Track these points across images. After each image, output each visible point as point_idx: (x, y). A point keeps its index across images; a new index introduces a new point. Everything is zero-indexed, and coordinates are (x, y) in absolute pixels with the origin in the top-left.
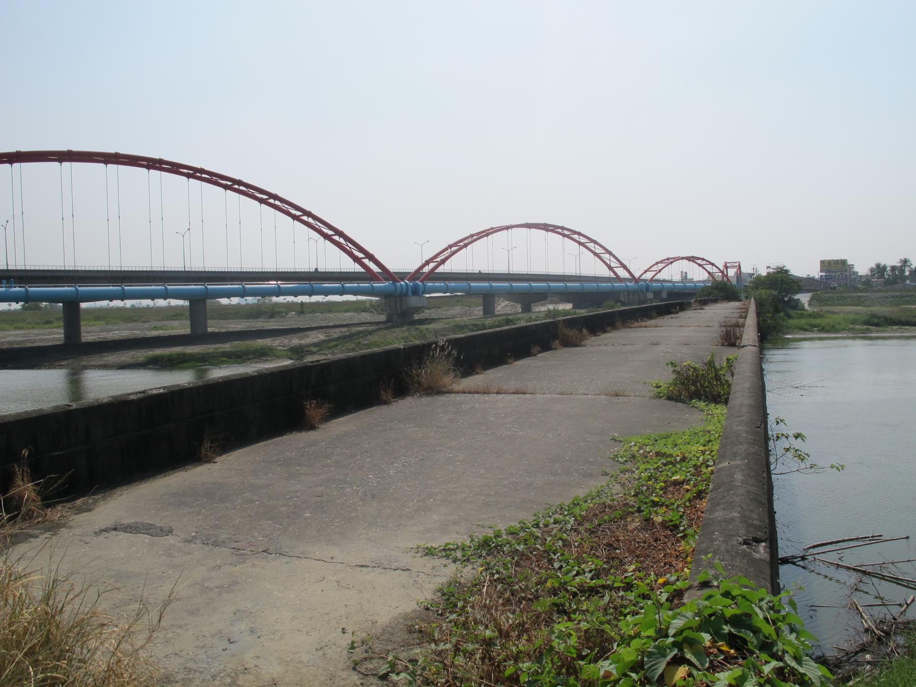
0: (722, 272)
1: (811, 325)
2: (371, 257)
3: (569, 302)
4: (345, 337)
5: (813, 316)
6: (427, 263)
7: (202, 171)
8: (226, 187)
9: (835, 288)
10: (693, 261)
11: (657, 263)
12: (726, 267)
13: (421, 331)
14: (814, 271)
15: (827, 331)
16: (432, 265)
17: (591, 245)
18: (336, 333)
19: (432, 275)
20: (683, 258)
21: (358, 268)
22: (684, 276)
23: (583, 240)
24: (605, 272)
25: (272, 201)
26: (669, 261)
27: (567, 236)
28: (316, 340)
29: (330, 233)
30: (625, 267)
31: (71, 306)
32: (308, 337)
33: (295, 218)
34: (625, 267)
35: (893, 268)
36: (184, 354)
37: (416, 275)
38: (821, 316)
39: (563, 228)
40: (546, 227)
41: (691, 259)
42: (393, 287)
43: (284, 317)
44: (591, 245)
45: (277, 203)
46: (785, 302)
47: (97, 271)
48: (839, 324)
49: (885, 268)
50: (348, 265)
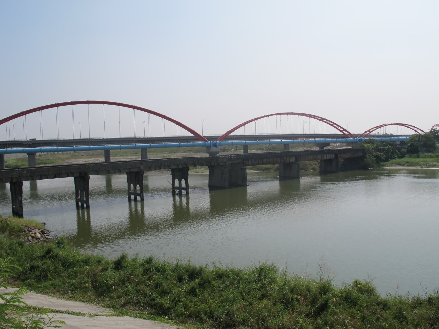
2: (346, 130)
6: (366, 132)
7: (314, 116)
8: (320, 120)
16: (367, 133)
19: (227, 137)
21: (341, 133)
27: (409, 128)
30: (422, 131)
31: (31, 154)
34: (422, 131)
47: (169, 137)
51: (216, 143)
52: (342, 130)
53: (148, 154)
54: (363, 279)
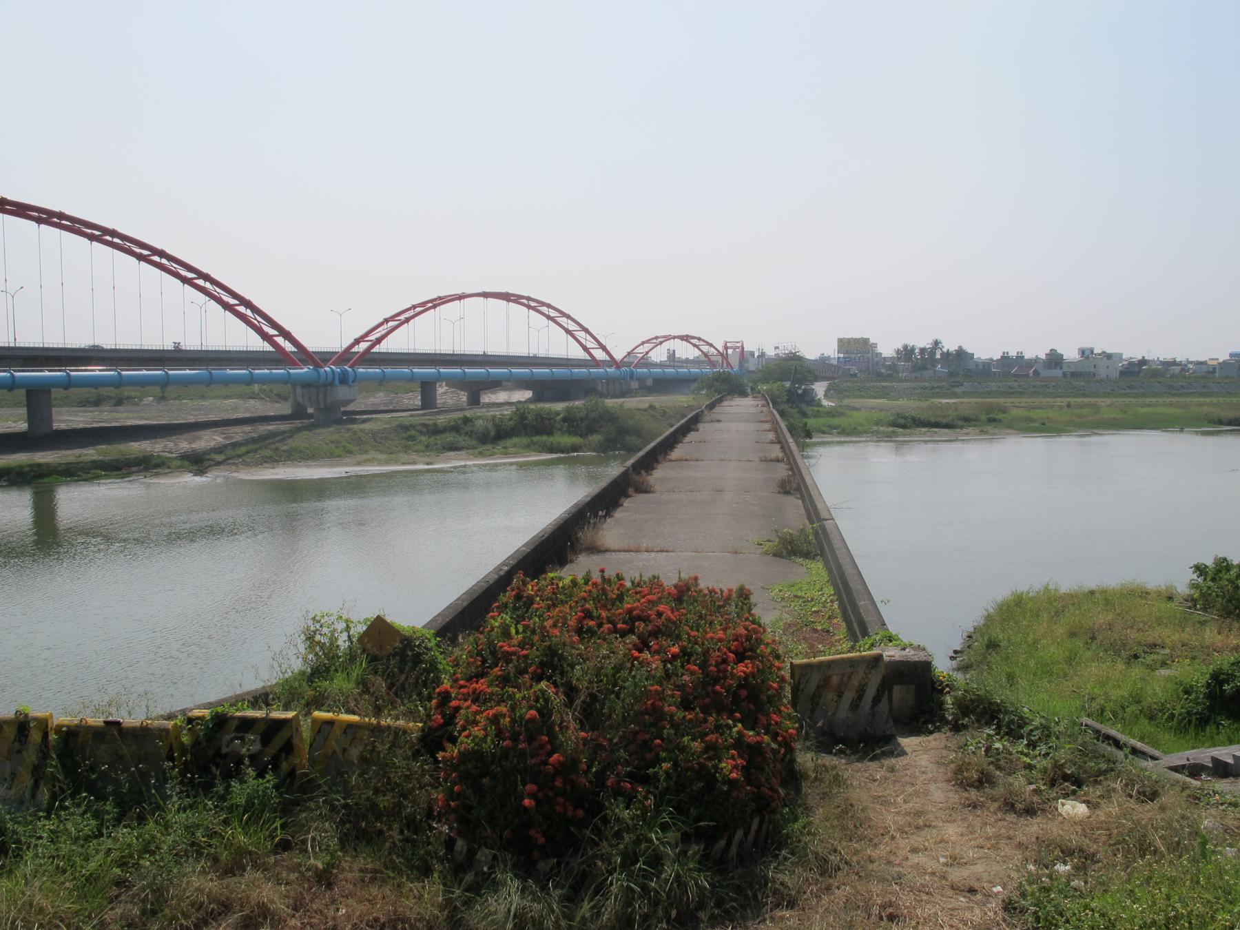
0: (722, 355)
1: (830, 426)
2: (287, 335)
3: (527, 388)
4: (254, 441)
5: (832, 413)
6: (357, 342)
7: (61, 216)
8: (92, 238)
9: (855, 375)
10: (687, 341)
11: (643, 343)
12: (726, 348)
13: (355, 433)
14: (831, 351)
15: (848, 434)
17: (563, 320)
18: (239, 434)
19: (367, 357)
20: (674, 337)
21: (268, 347)
22: (672, 355)
23: (553, 313)
24: (577, 353)
25: (156, 258)
26: (658, 341)
27: (534, 308)
28: (212, 444)
29: (233, 301)
30: (604, 348)
32: (200, 438)
33: (185, 280)
34: (604, 348)
35: (923, 350)
36: (39, 465)
37: (345, 356)
38: (840, 414)
39: (529, 299)
40: (506, 297)
41: (682, 338)
42: (315, 373)
43: (136, 404)
44: (563, 320)
45: (164, 261)
46: (798, 395)
48: (861, 425)
49: (913, 349)
50: (256, 344)
51: (344, 373)
52: (272, 332)
53: (54, 409)
54: (1003, 592)
